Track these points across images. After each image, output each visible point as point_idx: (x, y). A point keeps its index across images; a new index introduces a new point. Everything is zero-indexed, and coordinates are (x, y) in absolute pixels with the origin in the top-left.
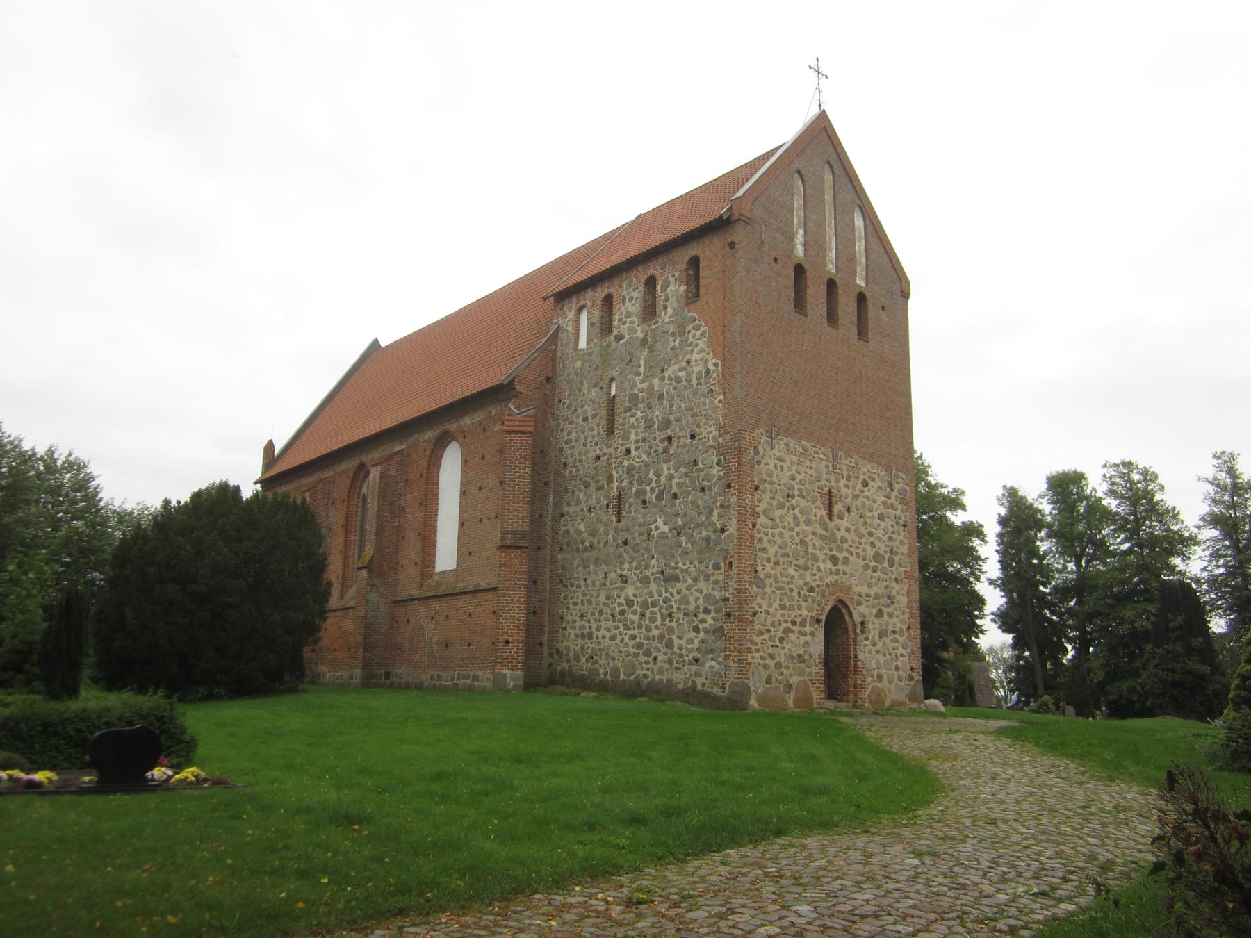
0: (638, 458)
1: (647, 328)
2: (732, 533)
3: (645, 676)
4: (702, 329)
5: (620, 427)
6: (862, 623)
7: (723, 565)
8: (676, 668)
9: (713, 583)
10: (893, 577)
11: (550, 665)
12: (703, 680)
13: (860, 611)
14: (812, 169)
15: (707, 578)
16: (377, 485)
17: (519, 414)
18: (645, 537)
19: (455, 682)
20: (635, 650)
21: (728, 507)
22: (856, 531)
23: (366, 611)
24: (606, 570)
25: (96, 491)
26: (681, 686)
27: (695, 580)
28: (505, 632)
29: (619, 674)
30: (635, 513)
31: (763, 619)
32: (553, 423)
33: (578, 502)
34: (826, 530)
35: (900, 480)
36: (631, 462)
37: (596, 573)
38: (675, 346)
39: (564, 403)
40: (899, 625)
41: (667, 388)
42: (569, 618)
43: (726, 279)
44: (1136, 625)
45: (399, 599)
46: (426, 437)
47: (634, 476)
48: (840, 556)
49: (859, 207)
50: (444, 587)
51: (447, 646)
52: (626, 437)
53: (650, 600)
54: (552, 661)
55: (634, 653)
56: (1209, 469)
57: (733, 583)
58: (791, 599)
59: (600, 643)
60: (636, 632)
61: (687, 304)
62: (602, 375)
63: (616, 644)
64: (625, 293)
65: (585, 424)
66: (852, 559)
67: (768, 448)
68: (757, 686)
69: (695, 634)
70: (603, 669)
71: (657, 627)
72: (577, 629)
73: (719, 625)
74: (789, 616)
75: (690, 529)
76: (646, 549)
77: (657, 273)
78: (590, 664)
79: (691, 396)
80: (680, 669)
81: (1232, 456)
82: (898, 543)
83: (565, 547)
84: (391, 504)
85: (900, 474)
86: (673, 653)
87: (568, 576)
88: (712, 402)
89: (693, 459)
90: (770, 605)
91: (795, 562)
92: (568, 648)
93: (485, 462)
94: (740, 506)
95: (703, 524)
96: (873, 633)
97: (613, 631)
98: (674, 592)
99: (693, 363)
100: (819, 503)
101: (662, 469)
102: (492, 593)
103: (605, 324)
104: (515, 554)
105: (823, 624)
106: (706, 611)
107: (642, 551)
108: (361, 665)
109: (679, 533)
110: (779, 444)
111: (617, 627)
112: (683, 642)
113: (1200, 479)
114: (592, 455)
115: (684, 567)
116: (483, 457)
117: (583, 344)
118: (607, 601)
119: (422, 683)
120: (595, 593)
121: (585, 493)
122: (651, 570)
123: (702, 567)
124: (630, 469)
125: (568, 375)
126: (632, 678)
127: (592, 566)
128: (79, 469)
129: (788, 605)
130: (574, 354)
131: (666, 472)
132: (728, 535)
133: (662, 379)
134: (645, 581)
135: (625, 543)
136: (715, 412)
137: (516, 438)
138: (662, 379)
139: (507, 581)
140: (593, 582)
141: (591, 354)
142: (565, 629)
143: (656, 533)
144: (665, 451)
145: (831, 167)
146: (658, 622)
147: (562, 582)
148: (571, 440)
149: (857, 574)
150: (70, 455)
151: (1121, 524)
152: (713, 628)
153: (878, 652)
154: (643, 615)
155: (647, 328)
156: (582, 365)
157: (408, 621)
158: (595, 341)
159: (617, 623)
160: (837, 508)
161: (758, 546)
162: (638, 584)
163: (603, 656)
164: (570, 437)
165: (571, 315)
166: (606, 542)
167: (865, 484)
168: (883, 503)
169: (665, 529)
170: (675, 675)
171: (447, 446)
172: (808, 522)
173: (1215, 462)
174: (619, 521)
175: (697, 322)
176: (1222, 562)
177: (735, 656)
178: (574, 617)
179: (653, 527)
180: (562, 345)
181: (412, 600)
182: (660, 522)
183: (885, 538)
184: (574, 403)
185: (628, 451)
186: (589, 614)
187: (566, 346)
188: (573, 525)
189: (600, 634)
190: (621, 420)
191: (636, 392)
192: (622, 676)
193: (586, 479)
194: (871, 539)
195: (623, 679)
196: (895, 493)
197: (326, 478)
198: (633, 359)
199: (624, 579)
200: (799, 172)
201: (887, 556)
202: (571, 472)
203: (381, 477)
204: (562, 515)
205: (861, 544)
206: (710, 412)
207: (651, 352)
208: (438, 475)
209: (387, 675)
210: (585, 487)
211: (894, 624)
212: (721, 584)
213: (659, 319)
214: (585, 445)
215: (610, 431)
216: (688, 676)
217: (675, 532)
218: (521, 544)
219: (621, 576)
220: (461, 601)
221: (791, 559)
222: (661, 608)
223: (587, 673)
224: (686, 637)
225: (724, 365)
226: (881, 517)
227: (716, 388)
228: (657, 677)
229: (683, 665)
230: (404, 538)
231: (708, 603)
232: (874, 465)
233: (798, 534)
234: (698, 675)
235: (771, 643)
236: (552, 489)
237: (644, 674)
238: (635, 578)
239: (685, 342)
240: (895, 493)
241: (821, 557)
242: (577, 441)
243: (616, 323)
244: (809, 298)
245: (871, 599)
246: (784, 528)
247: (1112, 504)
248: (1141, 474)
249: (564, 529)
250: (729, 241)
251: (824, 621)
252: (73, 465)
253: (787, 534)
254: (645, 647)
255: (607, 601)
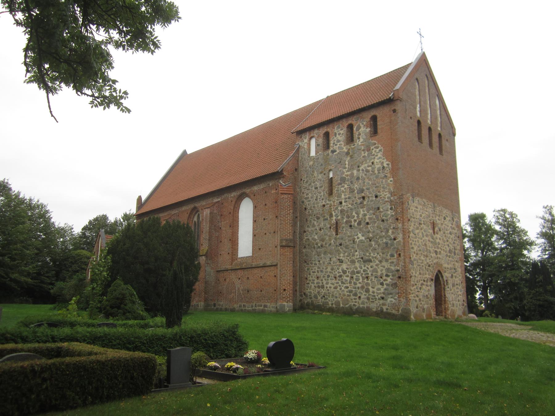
0: (346, 206)
1: (349, 147)
2: (400, 241)
3: (354, 305)
4: (380, 148)
5: (335, 192)
6: (447, 280)
7: (395, 255)
8: (372, 302)
9: (390, 263)
10: (456, 260)
11: (301, 300)
12: (387, 307)
13: (446, 275)
14: (421, 78)
15: (387, 260)
16: (208, 217)
17: (285, 185)
18: (352, 242)
19: (254, 308)
20: (348, 293)
21: (397, 229)
22: (443, 239)
23: (205, 275)
24: (330, 257)
25: (50, 218)
26: (374, 310)
27: (381, 262)
28: (284, 285)
29: (340, 304)
30: (345, 231)
31: (414, 279)
32: (298, 190)
33: (314, 226)
34: (433, 239)
35: (456, 217)
36: (342, 208)
37: (325, 258)
38: (365, 156)
39: (304, 181)
40: (458, 281)
41: (361, 174)
42: (311, 278)
43: (392, 126)
44: (512, 280)
45: (219, 269)
46: (232, 195)
47: (344, 214)
48: (438, 250)
49: (437, 95)
50: (245, 264)
51: (248, 291)
52: (339, 196)
53: (356, 271)
54: (302, 298)
55: (348, 295)
56: (541, 212)
57: (401, 263)
58: (423, 270)
59: (328, 290)
60: (348, 285)
61: (371, 137)
62: (325, 168)
63: (338, 291)
64: (336, 131)
65: (316, 190)
66: (442, 252)
67: (412, 203)
68: (413, 310)
69: (381, 286)
70: (331, 302)
71: (360, 283)
72: (315, 284)
73: (394, 282)
74: (422, 277)
75: (376, 238)
76: (353, 248)
77: (354, 122)
78: (323, 300)
79: (375, 178)
80: (373, 302)
81: (551, 208)
82: (456, 245)
83: (307, 246)
84: (215, 226)
85: (456, 214)
86: (369, 295)
87: (309, 260)
88: (386, 181)
89: (377, 207)
90: (416, 273)
91: (423, 254)
92: (310, 292)
93: (267, 207)
94: (404, 228)
95: (384, 236)
96: (450, 285)
97: (335, 285)
98: (369, 267)
99: (375, 163)
100: (430, 227)
101: (360, 211)
102: (273, 267)
103: (325, 145)
104: (287, 249)
105: (434, 281)
106: (387, 276)
107: (350, 248)
108: (203, 300)
109: (370, 241)
110: (416, 200)
111: (337, 283)
112: (375, 290)
113: (537, 217)
114: (321, 204)
115: (374, 256)
116: (266, 205)
117: (313, 153)
118: (331, 271)
119: (234, 308)
120: (325, 268)
121: (317, 222)
122: (355, 257)
123: (384, 256)
124: (342, 211)
125: (306, 168)
126: (347, 306)
127: (322, 255)
128: (42, 207)
129: (422, 272)
130: (308, 158)
131: (362, 212)
132: (398, 241)
133: (359, 170)
134: (353, 262)
135: (341, 245)
136: (389, 186)
137: (286, 196)
138: (359, 170)
139: (284, 262)
140: (324, 263)
141: (318, 159)
142: (309, 283)
143: (358, 240)
144: (361, 203)
145: (427, 77)
146: (361, 280)
147: (306, 262)
148: (308, 198)
149: (444, 258)
150: (38, 201)
151: (501, 236)
152: (391, 283)
153: (452, 293)
154: (352, 277)
155: (349, 147)
156: (314, 163)
157: (225, 280)
158: (320, 153)
159: (337, 281)
160: (436, 229)
161: (411, 246)
162: (349, 263)
163: (331, 296)
164: (308, 196)
165: (306, 141)
166: (330, 244)
167: (445, 219)
168: (451, 227)
169: (363, 238)
170: (371, 305)
171: (243, 200)
172: (427, 236)
173: (544, 210)
174: (337, 234)
175: (376, 145)
176: (547, 253)
177: (404, 296)
178: (313, 278)
179: (356, 237)
180: (301, 154)
181: (227, 270)
182: (360, 235)
183: (452, 243)
184: (309, 181)
185: (341, 203)
186: (322, 277)
187: (304, 154)
188: (311, 236)
189: (328, 286)
190: (336, 189)
191: (344, 176)
192: (341, 305)
193: (318, 215)
194: (448, 243)
195: (342, 307)
196: (454, 223)
197: (175, 214)
198: (342, 161)
199: (341, 261)
200: (417, 79)
201: (453, 250)
202: (309, 212)
203: (210, 213)
204: (305, 232)
205: (444, 245)
206: (386, 186)
207: (352, 158)
208: (238, 213)
209: (215, 305)
210: (317, 219)
211: (457, 281)
212: (395, 263)
213: (356, 143)
214: (316, 200)
215: (331, 193)
216: (378, 305)
217: (368, 240)
218: (290, 245)
219: (339, 260)
220: (256, 271)
221: (422, 252)
222: (362, 274)
223: (322, 304)
224: (376, 287)
225: (392, 163)
226: (451, 233)
227: (389, 175)
228: (361, 306)
229: (376, 300)
230: (221, 242)
231: (388, 272)
232: (447, 210)
233: (424, 241)
234: (384, 304)
235: (417, 290)
236: (299, 220)
237: (354, 304)
238: (347, 260)
239: (370, 154)
240: (454, 223)
241: (432, 251)
242: (311, 198)
243: (332, 145)
244: (423, 135)
245: (449, 270)
246: (419, 238)
247: (497, 228)
248: (510, 215)
249: (306, 238)
250: (393, 108)
251: (434, 280)
252: (40, 206)
253: (420, 241)
254: (354, 292)
255: (331, 271)
